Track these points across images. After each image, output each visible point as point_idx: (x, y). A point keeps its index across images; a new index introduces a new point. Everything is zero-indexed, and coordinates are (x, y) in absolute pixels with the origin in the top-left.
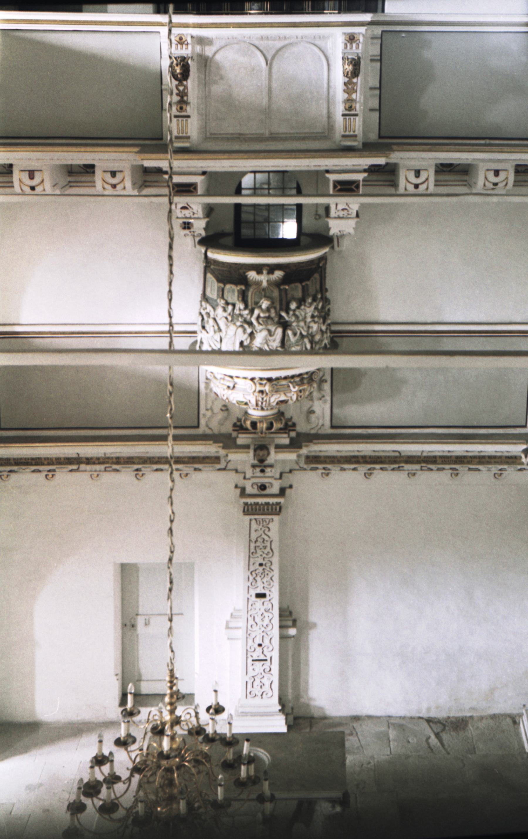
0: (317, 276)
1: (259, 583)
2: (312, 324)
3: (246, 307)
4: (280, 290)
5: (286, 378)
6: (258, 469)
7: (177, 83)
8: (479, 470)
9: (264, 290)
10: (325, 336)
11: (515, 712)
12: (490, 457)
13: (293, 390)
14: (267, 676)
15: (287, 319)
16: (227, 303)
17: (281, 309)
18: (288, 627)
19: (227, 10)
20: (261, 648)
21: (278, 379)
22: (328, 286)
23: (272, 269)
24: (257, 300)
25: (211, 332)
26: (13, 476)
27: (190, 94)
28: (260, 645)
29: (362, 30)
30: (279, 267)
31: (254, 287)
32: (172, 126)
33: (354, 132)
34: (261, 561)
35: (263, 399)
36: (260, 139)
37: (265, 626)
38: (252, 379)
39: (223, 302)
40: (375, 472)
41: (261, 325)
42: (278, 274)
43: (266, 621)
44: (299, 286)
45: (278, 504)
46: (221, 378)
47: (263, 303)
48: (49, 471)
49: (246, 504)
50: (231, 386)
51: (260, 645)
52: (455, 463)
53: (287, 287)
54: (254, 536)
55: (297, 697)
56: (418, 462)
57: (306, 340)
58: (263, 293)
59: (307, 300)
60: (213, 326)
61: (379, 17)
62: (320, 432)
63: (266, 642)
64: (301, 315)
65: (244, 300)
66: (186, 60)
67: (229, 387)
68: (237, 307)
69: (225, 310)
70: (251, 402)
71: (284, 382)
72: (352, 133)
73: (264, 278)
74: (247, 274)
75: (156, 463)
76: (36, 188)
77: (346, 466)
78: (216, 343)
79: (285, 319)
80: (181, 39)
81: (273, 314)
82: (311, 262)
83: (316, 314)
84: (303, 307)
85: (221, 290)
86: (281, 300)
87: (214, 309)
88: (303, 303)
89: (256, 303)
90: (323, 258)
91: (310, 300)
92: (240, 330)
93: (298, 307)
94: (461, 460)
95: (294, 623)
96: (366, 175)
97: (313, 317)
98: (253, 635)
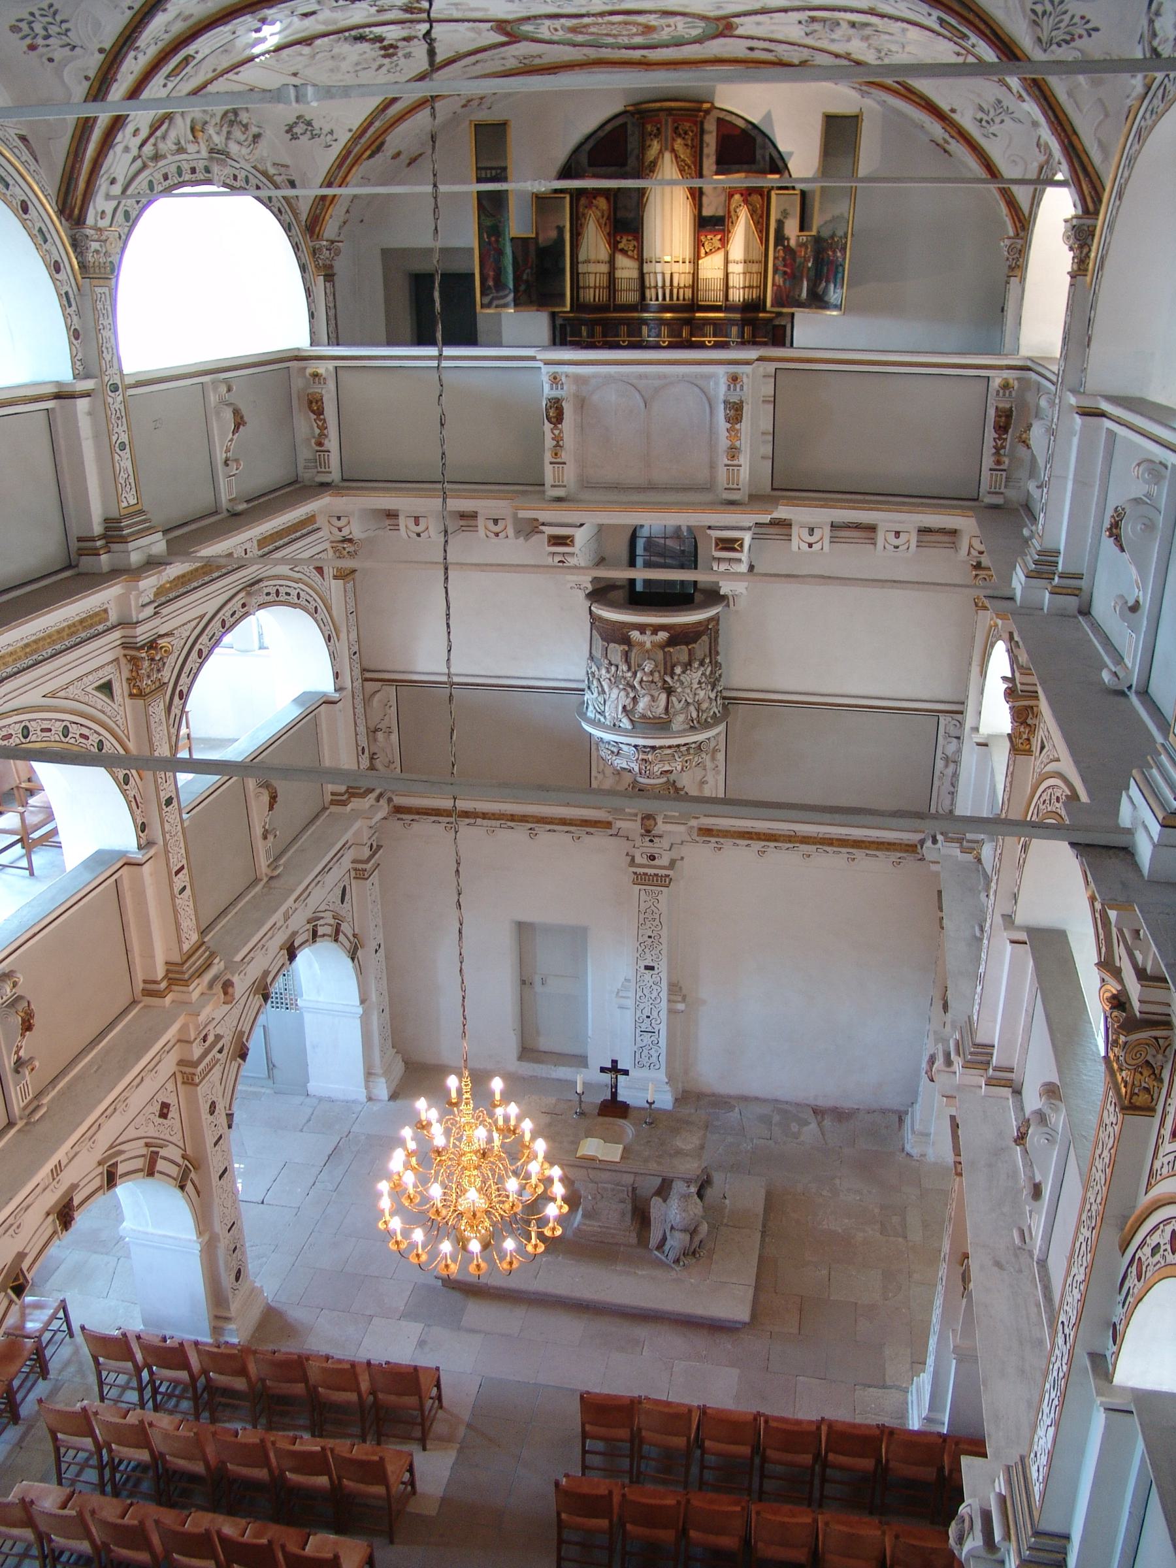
0: (705, 638)
1: (648, 956)
2: (699, 691)
3: (629, 669)
4: (665, 653)
5: (670, 747)
10: (714, 703)
12: (889, 844)
17: (665, 673)
21: (661, 747)
22: (720, 649)
23: (656, 629)
25: (596, 694)
26: (414, 824)
30: (663, 627)
36: (639, 489)
38: (635, 746)
42: (663, 636)
43: (655, 994)
44: (684, 647)
49: (635, 873)
50: (615, 750)
52: (853, 847)
54: (643, 906)
57: (692, 708)
63: (655, 1014)
65: (627, 661)
67: (613, 752)
69: (608, 672)
71: (669, 751)
72: (735, 486)
73: (647, 639)
77: (738, 841)
80: (555, 378)
82: (700, 623)
86: (665, 664)
89: (639, 666)
90: (715, 619)
91: (696, 665)
92: (623, 694)
93: (684, 672)
94: (858, 844)
95: (684, 1000)
97: (700, 683)
98: (641, 1006)
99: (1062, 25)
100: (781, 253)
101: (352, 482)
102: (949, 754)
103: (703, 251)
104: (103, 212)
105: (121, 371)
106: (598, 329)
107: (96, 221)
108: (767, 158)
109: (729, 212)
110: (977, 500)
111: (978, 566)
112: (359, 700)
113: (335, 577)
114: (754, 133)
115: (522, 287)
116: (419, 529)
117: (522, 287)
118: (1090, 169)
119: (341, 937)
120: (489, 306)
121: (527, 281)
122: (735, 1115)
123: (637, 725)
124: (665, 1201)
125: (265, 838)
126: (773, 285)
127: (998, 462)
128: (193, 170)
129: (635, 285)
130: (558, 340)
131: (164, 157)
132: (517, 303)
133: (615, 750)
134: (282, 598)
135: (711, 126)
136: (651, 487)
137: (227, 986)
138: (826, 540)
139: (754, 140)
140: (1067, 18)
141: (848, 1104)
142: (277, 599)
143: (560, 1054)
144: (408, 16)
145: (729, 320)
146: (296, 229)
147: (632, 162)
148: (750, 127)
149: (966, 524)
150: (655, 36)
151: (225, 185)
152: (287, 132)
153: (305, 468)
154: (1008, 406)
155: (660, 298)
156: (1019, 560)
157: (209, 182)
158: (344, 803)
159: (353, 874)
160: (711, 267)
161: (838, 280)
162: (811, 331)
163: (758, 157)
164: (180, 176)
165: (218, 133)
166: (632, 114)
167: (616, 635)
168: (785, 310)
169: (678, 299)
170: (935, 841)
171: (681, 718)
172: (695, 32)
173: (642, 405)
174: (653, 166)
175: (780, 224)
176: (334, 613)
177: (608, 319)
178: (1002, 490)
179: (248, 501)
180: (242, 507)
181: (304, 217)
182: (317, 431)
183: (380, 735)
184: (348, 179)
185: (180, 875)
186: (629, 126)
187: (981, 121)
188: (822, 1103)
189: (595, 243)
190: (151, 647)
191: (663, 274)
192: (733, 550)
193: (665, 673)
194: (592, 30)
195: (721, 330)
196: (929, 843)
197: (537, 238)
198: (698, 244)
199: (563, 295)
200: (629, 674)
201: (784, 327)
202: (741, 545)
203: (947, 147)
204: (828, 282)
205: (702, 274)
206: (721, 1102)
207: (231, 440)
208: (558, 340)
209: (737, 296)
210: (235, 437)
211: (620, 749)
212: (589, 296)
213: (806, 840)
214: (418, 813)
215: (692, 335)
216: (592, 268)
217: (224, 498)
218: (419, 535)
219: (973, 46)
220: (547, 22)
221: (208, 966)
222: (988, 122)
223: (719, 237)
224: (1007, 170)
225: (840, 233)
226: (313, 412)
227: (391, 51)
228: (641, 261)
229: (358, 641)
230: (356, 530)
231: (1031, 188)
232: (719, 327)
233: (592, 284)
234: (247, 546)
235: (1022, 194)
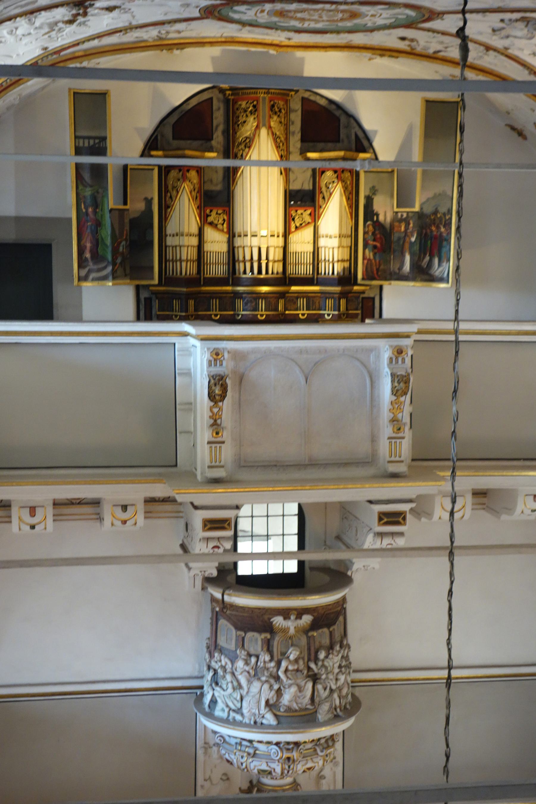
4: (309, 638)
9: (291, 638)
17: (309, 660)
19: (216, 310)
23: (300, 612)
24: (284, 650)
25: (230, 690)
27: (223, 417)
31: (280, 634)
33: (400, 457)
35: (289, 767)
38: (277, 744)
39: (244, 653)
41: (290, 679)
42: (307, 619)
44: (325, 630)
46: (236, 743)
47: (291, 653)
50: (251, 751)
53: (315, 634)
57: (335, 695)
58: (290, 642)
59: (335, 648)
60: (232, 682)
64: (329, 665)
66: (224, 379)
67: (249, 754)
68: (261, 658)
69: (247, 663)
70: (276, 770)
72: (397, 459)
73: (291, 625)
74: (272, 620)
76: (36, 527)
78: (235, 702)
79: (313, 671)
84: (331, 656)
85: (240, 640)
86: (309, 649)
87: (233, 663)
88: (331, 651)
89: (283, 654)
90: (344, 600)
91: (338, 648)
92: (266, 686)
97: (340, 667)
100: (371, 228)
106: (191, 303)
108: (353, 137)
114: (338, 113)
115: (119, 261)
117: (119, 261)
121: (123, 253)
126: (364, 258)
133: (251, 751)
135: (296, 105)
136: (312, 464)
138: (50, 519)
148: (333, 107)
160: (302, 242)
161: (443, 254)
163: (342, 136)
169: (272, 273)
171: (325, 707)
173: (302, 380)
174: (248, 143)
175: (369, 201)
177: (200, 293)
189: (185, 214)
192: (397, 523)
193: (309, 660)
195: (314, 303)
198: (288, 219)
199: (152, 268)
200: (273, 664)
201: (373, 299)
202: (229, 525)
204: (432, 256)
211: (256, 749)
215: (286, 309)
223: (309, 212)
225: (443, 210)
228: (232, 235)
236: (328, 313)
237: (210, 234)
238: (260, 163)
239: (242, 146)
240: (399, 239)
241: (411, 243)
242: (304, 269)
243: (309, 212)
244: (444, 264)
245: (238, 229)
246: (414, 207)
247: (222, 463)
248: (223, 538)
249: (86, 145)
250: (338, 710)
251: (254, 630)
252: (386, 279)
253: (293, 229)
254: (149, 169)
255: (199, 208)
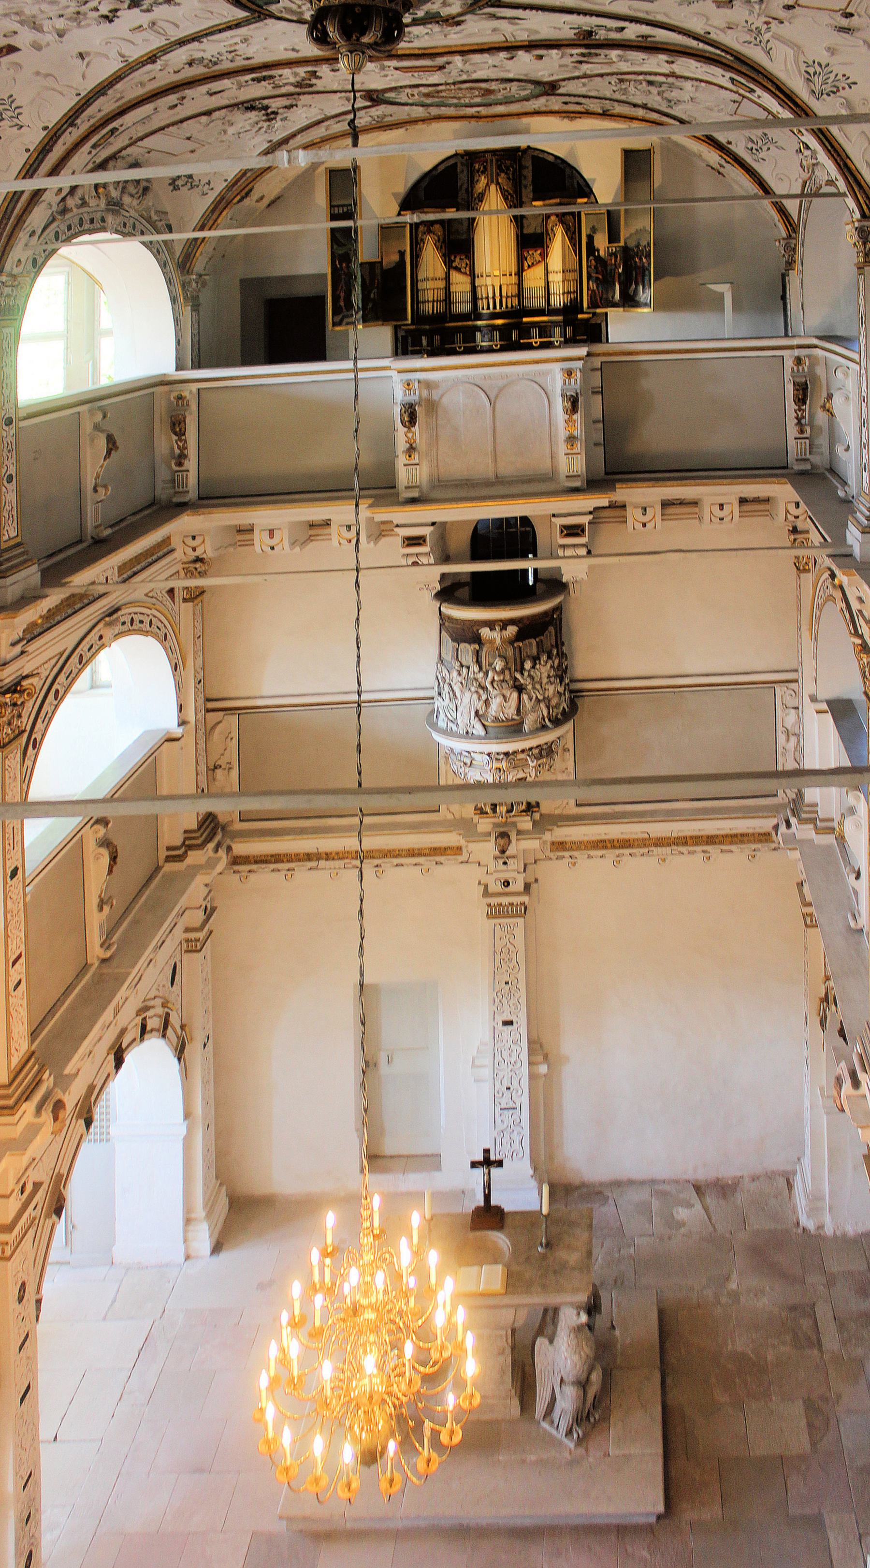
0: (551, 629)
3: (481, 668)
6: (501, 861)
7: (406, 429)
8: (732, 851)
11: (789, 1168)
12: (742, 835)
13: (531, 764)
14: (517, 1130)
15: (522, 681)
16: (462, 666)
17: (516, 670)
18: (537, 1064)
20: (509, 1092)
21: (515, 752)
23: (505, 624)
24: (491, 661)
25: (447, 700)
26: (252, 877)
27: (418, 441)
28: (508, 1088)
29: (580, 364)
32: (403, 476)
34: (507, 979)
37: (513, 1062)
38: (489, 755)
40: (624, 859)
42: (512, 630)
43: (514, 1054)
44: (534, 642)
45: (523, 904)
48: (288, 870)
49: (489, 905)
50: (469, 762)
51: (508, 1088)
52: (707, 844)
53: (521, 644)
55: (551, 1157)
56: (669, 845)
57: (542, 705)
61: (598, 348)
62: (564, 813)
65: (478, 662)
67: (465, 764)
68: (471, 670)
69: (460, 674)
75: (396, 857)
77: (593, 853)
81: (508, 677)
82: (545, 614)
83: (552, 673)
84: (538, 666)
89: (490, 665)
90: (558, 608)
91: (544, 657)
92: (475, 696)
94: (711, 840)
96: (591, 517)
97: (549, 677)
99: (830, 81)
101: (212, 497)
102: (789, 727)
103: (526, 265)
104: (19, 261)
105: (16, 405)
106: (437, 338)
107: (12, 269)
108: (575, 184)
109: (547, 231)
110: (786, 467)
111: (795, 530)
112: (201, 732)
113: (185, 600)
115: (370, 305)
116: (272, 542)
117: (370, 305)
118: (863, 183)
119: (170, 1031)
120: (340, 324)
122: (608, 1210)
123: (489, 730)
124: (551, 1342)
125: (101, 909)
126: (588, 289)
127: (802, 432)
128: (92, 221)
129: (468, 297)
130: (400, 351)
131: (71, 210)
132: (365, 320)
134: (137, 625)
137: (59, 1105)
139: (563, 171)
140: (832, 76)
141: (728, 1172)
142: (134, 627)
143: (408, 1157)
144: (298, 90)
145: (552, 322)
146: (171, 266)
147: (462, 194)
148: (559, 161)
149: (783, 492)
150: (492, 97)
151: (117, 232)
152: (170, 184)
153: (163, 488)
154: (803, 380)
155: (504, 306)
156: (850, 517)
157: (103, 229)
158: (180, 858)
159: (185, 945)
160: (534, 278)
162: (628, 328)
164: (81, 225)
165: (116, 189)
166: (462, 156)
167: (468, 634)
168: (598, 311)
170: (788, 825)
172: (524, 93)
174: (481, 197)
175: (590, 239)
176: (182, 639)
178: (808, 456)
179: (111, 526)
180: (107, 532)
181: (178, 254)
182: (177, 451)
183: (219, 772)
184: (219, 221)
185: (17, 965)
186: (459, 165)
187: (752, 149)
188: (702, 1175)
189: (432, 262)
190: (15, 691)
191: (493, 287)
194: (443, 94)
195: (545, 332)
196: (783, 828)
197: (381, 262)
198: (521, 259)
201: (600, 325)
202: (424, 541)
203: (721, 170)
204: (637, 285)
205: (527, 284)
206: (594, 1192)
207: (102, 467)
208: (400, 351)
209: (557, 301)
210: (105, 463)
211: (472, 759)
212: (428, 308)
213: (660, 842)
214: (256, 862)
215: (520, 338)
216: (430, 284)
217: (90, 523)
218: (272, 548)
219: (759, 97)
220: (408, 90)
221: (37, 1083)
222: (757, 150)
223: (539, 252)
224: (779, 188)
225: (644, 243)
226: (175, 434)
227: (272, 116)
228: (473, 275)
229: (203, 668)
230: (207, 550)
231: (798, 201)
232: (544, 330)
233: (431, 299)
234: (109, 573)
235: (792, 206)
236: (557, 339)
237: (455, 276)
238: (490, 213)
239: (477, 201)
240: (611, 270)
241: (619, 274)
242: (539, 302)
243: (539, 252)
244: (647, 291)
245: (477, 271)
246: (619, 242)
247: (418, 483)
248: (421, 554)
249: (341, 211)
250: (547, 720)
251: (465, 642)
252: (607, 306)
253: (526, 268)
254: (400, 226)
255: (444, 256)
